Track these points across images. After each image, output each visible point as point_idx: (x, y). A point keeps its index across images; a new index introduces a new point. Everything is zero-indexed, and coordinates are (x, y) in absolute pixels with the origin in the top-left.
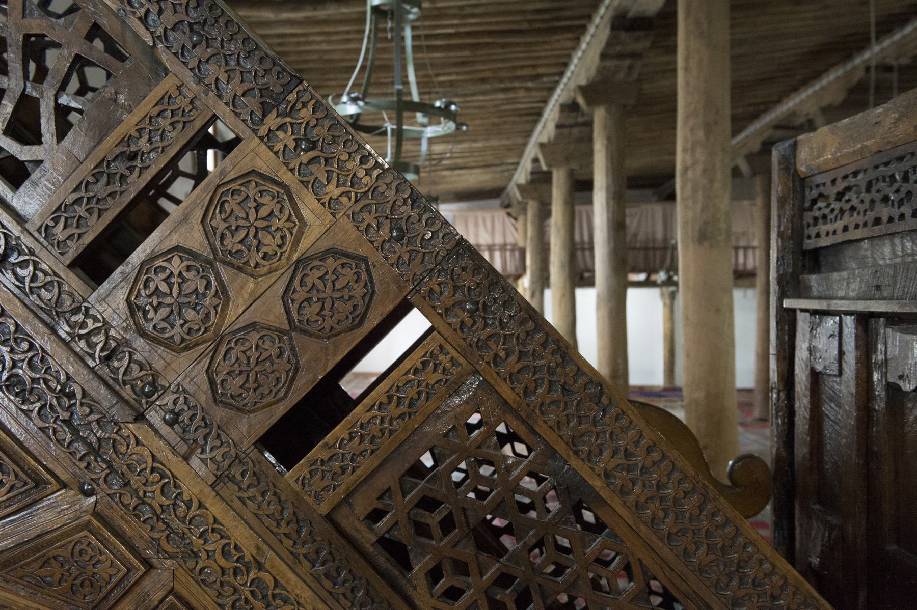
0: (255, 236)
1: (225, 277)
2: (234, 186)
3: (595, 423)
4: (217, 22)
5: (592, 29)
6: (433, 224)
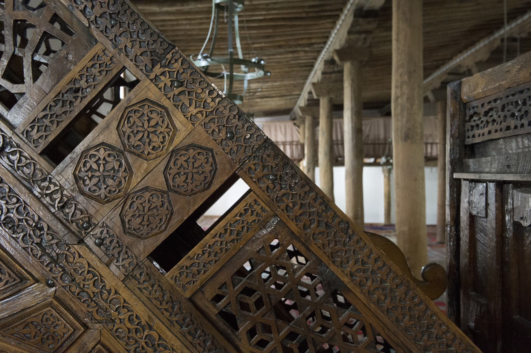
0: (148, 137)
1: (130, 161)
2: (135, 108)
3: (344, 245)
4: (125, 12)
5: (343, 17)
6: (251, 130)
